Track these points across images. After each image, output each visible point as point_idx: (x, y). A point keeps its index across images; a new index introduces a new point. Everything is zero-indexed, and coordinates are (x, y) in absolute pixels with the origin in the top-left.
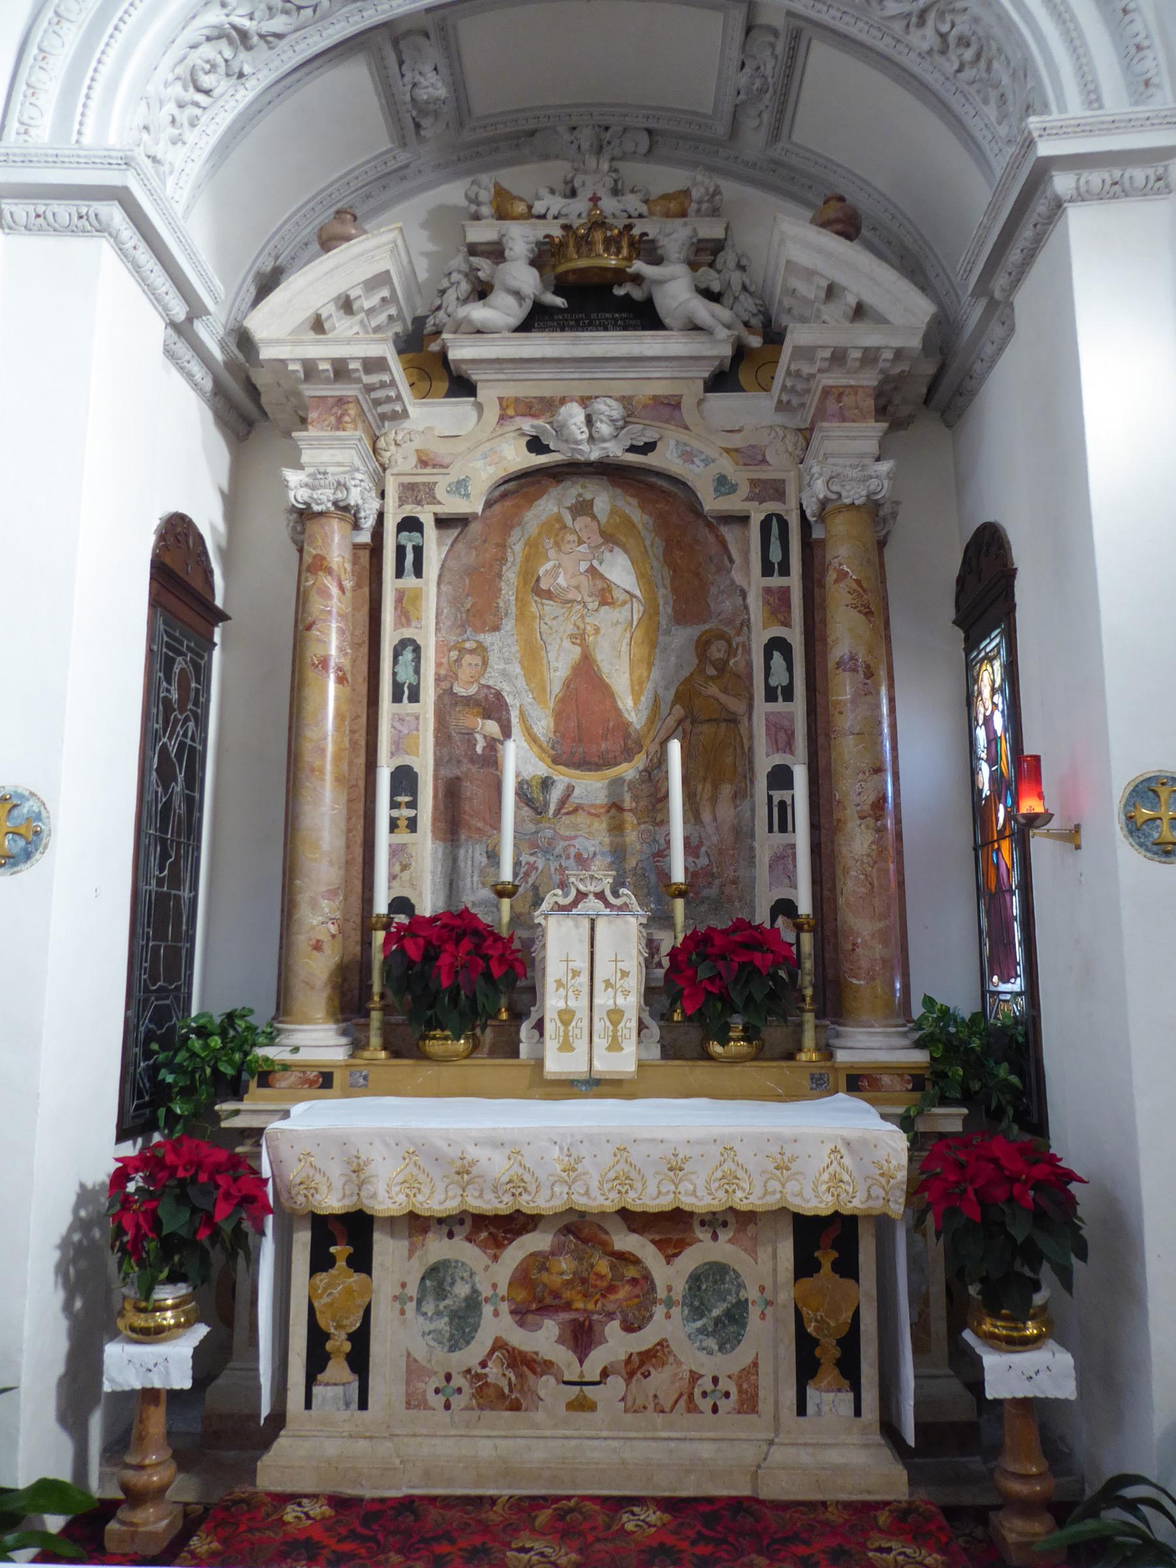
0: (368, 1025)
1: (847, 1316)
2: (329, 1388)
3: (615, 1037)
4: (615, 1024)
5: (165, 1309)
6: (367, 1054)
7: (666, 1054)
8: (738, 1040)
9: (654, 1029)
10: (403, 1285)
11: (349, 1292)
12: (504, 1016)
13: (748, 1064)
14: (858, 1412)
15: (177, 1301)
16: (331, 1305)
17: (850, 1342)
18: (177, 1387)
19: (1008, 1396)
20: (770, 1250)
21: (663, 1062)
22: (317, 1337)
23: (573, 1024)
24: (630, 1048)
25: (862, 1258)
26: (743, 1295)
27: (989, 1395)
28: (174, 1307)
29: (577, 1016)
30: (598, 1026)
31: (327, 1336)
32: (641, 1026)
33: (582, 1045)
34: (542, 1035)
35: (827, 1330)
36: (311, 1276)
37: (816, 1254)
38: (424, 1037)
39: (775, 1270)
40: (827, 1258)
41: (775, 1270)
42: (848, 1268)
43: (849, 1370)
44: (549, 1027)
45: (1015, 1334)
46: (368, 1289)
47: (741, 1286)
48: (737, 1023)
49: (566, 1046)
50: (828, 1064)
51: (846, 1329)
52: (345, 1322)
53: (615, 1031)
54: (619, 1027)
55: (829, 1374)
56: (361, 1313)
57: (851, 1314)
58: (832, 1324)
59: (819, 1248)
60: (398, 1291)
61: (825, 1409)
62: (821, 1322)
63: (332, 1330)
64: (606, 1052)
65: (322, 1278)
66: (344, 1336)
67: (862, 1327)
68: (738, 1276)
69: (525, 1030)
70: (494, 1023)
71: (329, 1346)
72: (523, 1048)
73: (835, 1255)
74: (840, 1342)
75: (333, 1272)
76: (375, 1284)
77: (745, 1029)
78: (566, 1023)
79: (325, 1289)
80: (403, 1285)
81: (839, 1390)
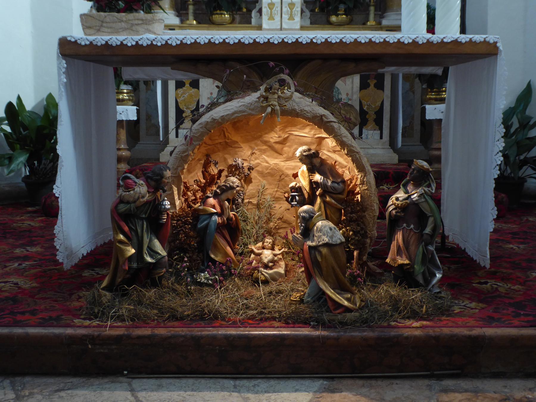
0: (188, 14)
1: (379, 104)
2: (184, 130)
3: (291, 15)
4: (291, 9)
5: (124, 93)
6: (188, 22)
7: (311, 23)
8: (343, 14)
9: (308, 13)
10: (211, 94)
11: (191, 96)
12: (245, 10)
13: (346, 26)
14: (381, 138)
15: (129, 91)
16: (184, 100)
17: (380, 113)
18: (131, 119)
19: (434, 118)
20: (351, 80)
21: (311, 26)
22: (179, 112)
23: (274, 9)
24: (298, 18)
25: (385, 83)
26: (340, 97)
27: (427, 117)
28: (127, 93)
29: (276, 5)
30: (284, 9)
31: (183, 112)
32: (302, 12)
33: (278, 18)
34: (261, 15)
35: (371, 108)
36: (176, 90)
37: (368, 81)
38: (212, 14)
39: (352, 87)
40: (372, 83)
41: (352, 87)
42: (380, 86)
43: (379, 123)
44: (264, 10)
45: (438, 97)
46: (198, 95)
47: (339, 93)
48: (342, 7)
49: (271, 18)
50: (379, 26)
51: (378, 108)
52: (190, 107)
53: (291, 12)
54: (293, 11)
55: (371, 124)
56: (196, 103)
57: (380, 103)
58: (373, 106)
59: (369, 79)
60: (209, 96)
61: (369, 137)
62: (369, 106)
63: (185, 109)
64: (288, 21)
65: (180, 91)
66: (189, 112)
67: (384, 108)
68: (338, 90)
69: (254, 13)
70: (240, 13)
71: (184, 115)
72: (253, 21)
73: (375, 81)
74: (376, 113)
75: (184, 88)
76: (201, 93)
77: (345, 11)
78: (271, 9)
79: (182, 95)
80: (211, 94)
81: (375, 130)
